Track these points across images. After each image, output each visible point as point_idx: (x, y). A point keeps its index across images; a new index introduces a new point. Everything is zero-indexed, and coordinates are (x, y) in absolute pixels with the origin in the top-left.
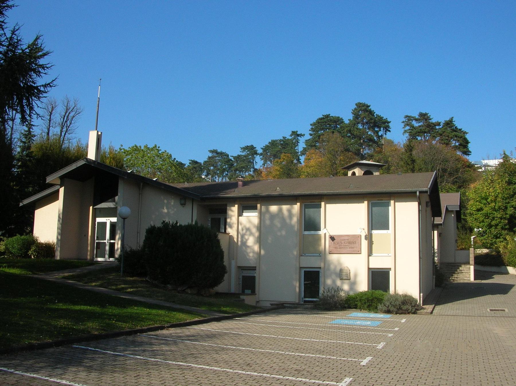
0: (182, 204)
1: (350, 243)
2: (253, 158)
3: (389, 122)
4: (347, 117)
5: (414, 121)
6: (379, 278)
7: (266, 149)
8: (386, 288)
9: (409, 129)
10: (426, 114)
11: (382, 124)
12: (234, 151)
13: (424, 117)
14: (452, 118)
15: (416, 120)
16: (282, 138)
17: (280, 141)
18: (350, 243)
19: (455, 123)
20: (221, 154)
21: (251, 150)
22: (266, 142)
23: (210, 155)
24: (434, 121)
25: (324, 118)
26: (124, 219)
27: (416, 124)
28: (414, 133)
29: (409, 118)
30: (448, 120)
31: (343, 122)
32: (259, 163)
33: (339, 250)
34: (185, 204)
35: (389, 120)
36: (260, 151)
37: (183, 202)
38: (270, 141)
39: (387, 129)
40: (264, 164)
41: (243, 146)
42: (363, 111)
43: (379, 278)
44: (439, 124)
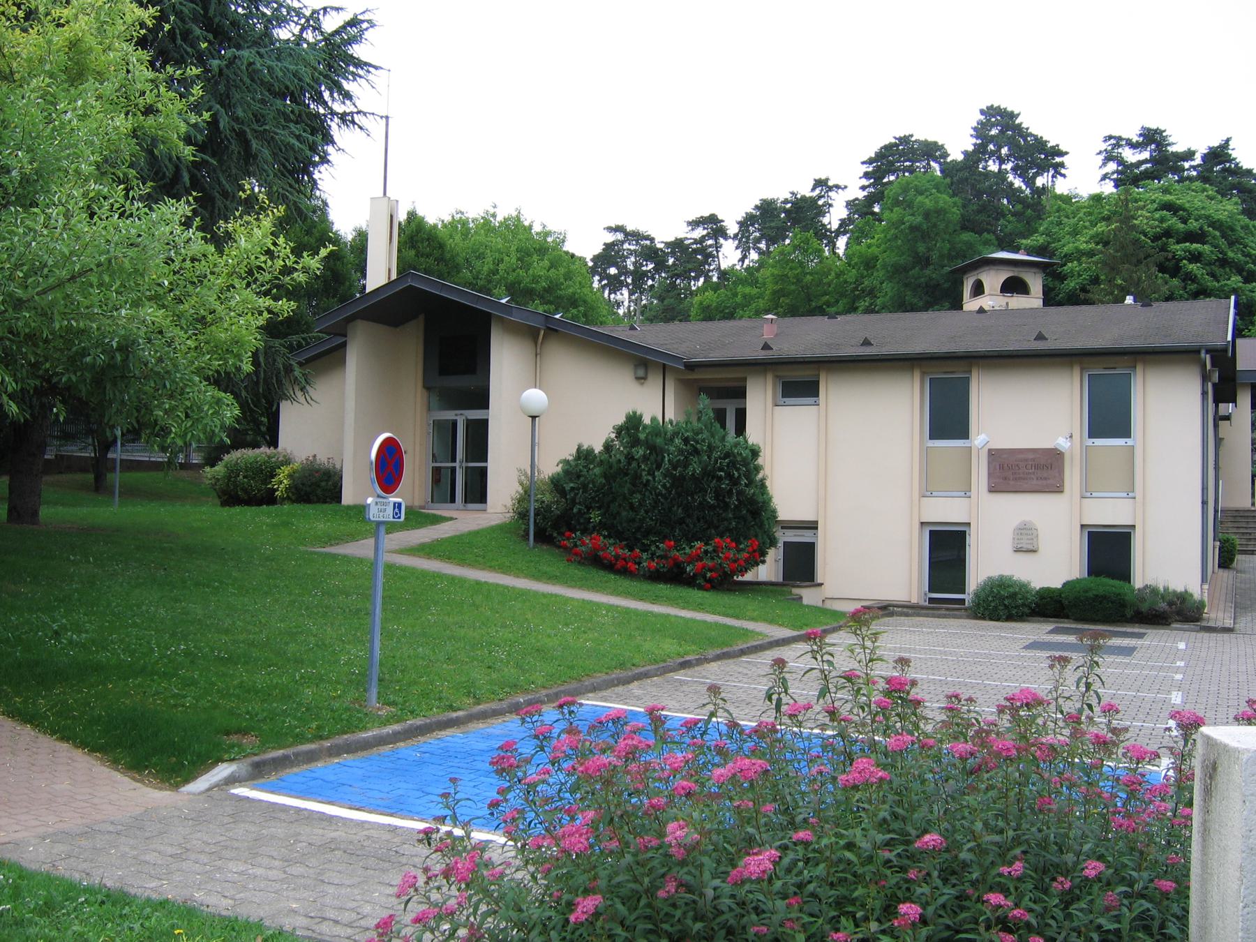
0: (638, 378)
1: (1037, 467)
2: (718, 247)
3: (975, 129)
4: (958, 144)
5: (1127, 148)
6: (1109, 549)
7: (745, 224)
8: (1126, 576)
9: (1117, 172)
10: (1158, 132)
11: (1041, 156)
12: (667, 228)
13: (1152, 137)
14: (1228, 140)
15: (1133, 145)
16: (788, 196)
17: (786, 202)
18: (1037, 467)
19: (1234, 154)
20: (636, 236)
21: (713, 226)
22: (748, 205)
23: (610, 238)
24: (1178, 148)
25: (896, 145)
26: (534, 418)
27: (1130, 156)
28: (1128, 177)
29: (1118, 141)
30: (1216, 144)
31: (946, 155)
32: (729, 255)
33: (1012, 483)
34: (645, 378)
35: (1063, 148)
36: (733, 229)
37: (641, 373)
38: (758, 203)
39: (1058, 169)
40: (742, 260)
41: (692, 218)
42: (1000, 128)
43: (1109, 549)
44: (1189, 155)
